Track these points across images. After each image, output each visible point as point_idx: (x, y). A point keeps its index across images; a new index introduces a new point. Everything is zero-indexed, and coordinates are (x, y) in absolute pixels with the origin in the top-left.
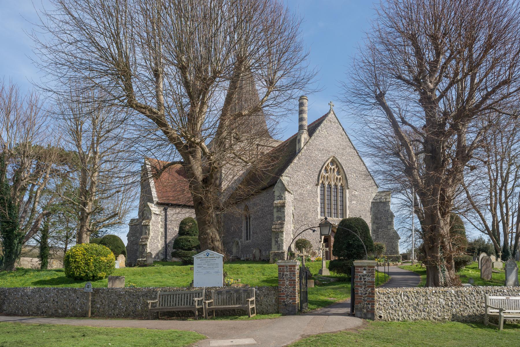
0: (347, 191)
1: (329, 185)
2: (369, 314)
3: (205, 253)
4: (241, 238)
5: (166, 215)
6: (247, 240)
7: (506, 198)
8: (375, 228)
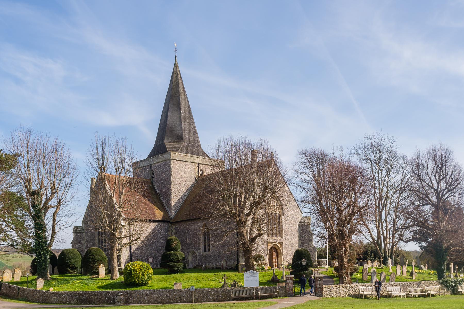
0: (283, 217)
1: (272, 213)
2: (321, 295)
3: (250, 271)
4: (198, 249)
5: (130, 229)
6: (205, 251)
7: (386, 217)
8: (301, 244)
